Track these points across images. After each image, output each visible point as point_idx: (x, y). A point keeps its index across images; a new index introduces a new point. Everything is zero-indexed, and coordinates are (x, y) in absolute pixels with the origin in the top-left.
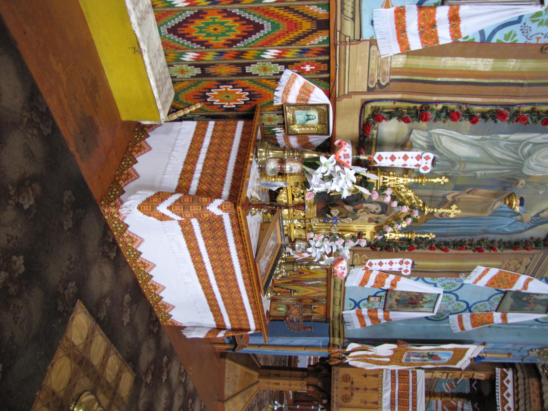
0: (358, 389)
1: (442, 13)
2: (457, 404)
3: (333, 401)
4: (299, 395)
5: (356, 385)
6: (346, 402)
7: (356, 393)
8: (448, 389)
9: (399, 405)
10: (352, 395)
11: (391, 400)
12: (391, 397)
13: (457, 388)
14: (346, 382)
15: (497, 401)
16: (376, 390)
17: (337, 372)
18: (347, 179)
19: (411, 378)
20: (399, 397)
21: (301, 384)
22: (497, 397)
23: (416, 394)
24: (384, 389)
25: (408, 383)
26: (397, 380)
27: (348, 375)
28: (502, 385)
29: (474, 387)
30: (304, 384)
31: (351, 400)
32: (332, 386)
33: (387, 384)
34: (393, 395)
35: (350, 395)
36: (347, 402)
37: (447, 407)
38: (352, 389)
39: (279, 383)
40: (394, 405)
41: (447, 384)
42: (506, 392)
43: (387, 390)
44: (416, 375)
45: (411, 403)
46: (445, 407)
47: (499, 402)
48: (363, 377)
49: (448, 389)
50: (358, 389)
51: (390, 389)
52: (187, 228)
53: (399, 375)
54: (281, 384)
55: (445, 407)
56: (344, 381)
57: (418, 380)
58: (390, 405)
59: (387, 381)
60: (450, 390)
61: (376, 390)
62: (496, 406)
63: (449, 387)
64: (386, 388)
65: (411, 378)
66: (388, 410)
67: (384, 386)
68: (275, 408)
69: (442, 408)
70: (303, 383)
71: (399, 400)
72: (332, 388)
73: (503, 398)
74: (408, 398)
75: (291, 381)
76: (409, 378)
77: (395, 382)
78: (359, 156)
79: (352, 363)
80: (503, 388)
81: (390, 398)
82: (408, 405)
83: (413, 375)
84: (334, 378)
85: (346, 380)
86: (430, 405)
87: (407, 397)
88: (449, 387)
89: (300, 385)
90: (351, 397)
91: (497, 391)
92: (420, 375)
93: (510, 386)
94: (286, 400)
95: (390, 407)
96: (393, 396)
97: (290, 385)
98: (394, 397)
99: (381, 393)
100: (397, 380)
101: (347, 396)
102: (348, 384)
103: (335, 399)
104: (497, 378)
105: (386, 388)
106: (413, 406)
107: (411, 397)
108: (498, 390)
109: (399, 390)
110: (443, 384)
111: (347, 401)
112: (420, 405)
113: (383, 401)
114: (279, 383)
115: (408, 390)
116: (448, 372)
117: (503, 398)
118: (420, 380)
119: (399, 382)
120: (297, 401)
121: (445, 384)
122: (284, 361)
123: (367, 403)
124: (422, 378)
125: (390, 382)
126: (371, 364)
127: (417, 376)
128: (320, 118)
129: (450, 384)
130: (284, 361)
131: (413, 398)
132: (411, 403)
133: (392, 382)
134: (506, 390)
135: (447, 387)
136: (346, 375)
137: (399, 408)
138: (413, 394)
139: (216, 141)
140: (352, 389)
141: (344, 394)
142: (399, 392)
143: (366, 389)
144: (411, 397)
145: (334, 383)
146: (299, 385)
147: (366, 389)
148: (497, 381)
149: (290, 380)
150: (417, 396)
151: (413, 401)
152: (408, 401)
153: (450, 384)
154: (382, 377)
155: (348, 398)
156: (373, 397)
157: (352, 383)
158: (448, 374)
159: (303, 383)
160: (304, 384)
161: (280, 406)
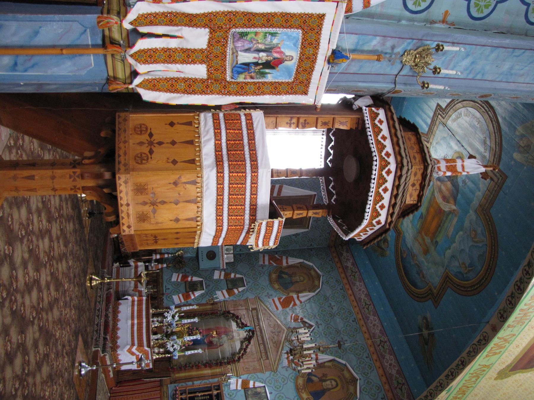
0: (160, 143)
3: (119, 163)
4: (122, 374)
5: (156, 138)
6: (142, 163)
7: (157, 149)
9: (229, 161)
10: (151, 152)
11: (216, 156)
12: (216, 151)
14: (141, 134)
15: (371, 146)
16: (191, 142)
17: (125, 120)
19: (244, 124)
20: (228, 150)
21: (72, 174)
22: (371, 142)
23: (255, 143)
24: (203, 140)
25: (241, 129)
26: (226, 165)
27: (144, 125)
28: (374, 126)
29: (332, 190)
30: (77, 174)
31: (150, 159)
32: (117, 139)
33: (208, 132)
34: (218, 149)
35: (148, 154)
36: (144, 163)
38: (151, 143)
39: (34, 176)
40: (222, 161)
42: (381, 135)
43: (209, 140)
44: (251, 119)
45: (247, 156)
47: (374, 148)
48: (168, 127)
50: (160, 143)
51: (213, 137)
53: (225, 120)
54: (36, 178)
56: (139, 134)
57: (255, 126)
58: (215, 163)
59: (207, 129)
61: (191, 142)
62: (364, 212)
64: (206, 138)
65: (244, 124)
66: (213, 169)
67: (202, 136)
68: (83, 372)
70: (74, 173)
71: (228, 154)
72: (117, 143)
73: (378, 142)
74: (243, 150)
75: (55, 171)
76: (241, 123)
77: (220, 129)
79: (148, 96)
80: (376, 130)
81: (214, 154)
82: (244, 160)
83: (247, 120)
84: (120, 129)
85: (141, 131)
87: (241, 149)
89: (70, 177)
90: (150, 156)
91: (369, 133)
92: (258, 119)
93: (384, 127)
94: (103, 375)
95: (215, 165)
96: (218, 149)
97: (53, 178)
98: (221, 151)
99: (199, 146)
100: (226, 165)
101: (143, 155)
102: (145, 138)
103: (122, 158)
104: (366, 118)
105: (206, 138)
106: (251, 161)
107: (246, 148)
108: (370, 132)
109: (227, 140)
111: (144, 162)
112: (262, 160)
113: (204, 157)
114: (34, 176)
115: (242, 140)
116: (298, 116)
117: (378, 142)
118: (257, 125)
119: (226, 129)
120: (120, 382)
122: (97, 325)
123: (177, 162)
124: (260, 123)
125: (213, 128)
126: (179, 95)
127: (253, 120)
131: (250, 150)
132: (247, 156)
133: (215, 129)
134: (380, 132)
136: (141, 125)
137: (229, 165)
138: (249, 144)
140: (151, 143)
141: (138, 152)
142: (227, 144)
143: (173, 143)
144: (246, 148)
145: (119, 135)
146: (68, 176)
147: (173, 143)
148: (367, 122)
149: (52, 169)
150: (257, 147)
151: (250, 154)
152: (244, 154)
154: (199, 123)
155: (146, 158)
156: (186, 153)
157: (151, 135)
158: (298, 119)
159: (74, 173)
160: (77, 174)
161: (90, 368)
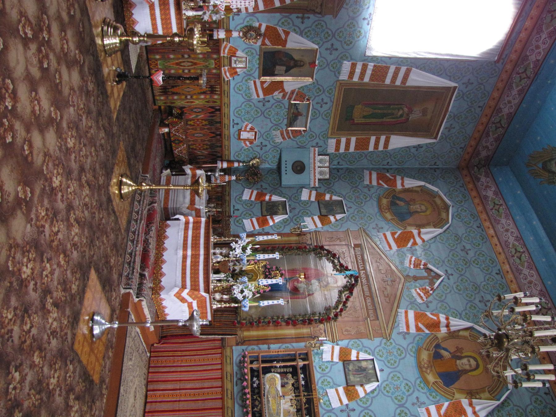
1: (342, 150)
2: (438, 318)
8: (421, 297)
13: (434, 294)
18: (105, 336)
37: (423, 324)
41: (418, 290)
46: (420, 325)
49: (421, 297)
52: (154, 22)
55: (420, 325)
60: (424, 298)
63: (422, 294)
69: (417, 326)
78: (229, 165)
86: (396, 324)
88: (422, 294)
110: (413, 291)
121: (416, 290)
122: (131, 254)
128: (133, 148)
129: (423, 289)
130: (131, 254)
135: (419, 294)
139: (162, 7)
153: (423, 289)
